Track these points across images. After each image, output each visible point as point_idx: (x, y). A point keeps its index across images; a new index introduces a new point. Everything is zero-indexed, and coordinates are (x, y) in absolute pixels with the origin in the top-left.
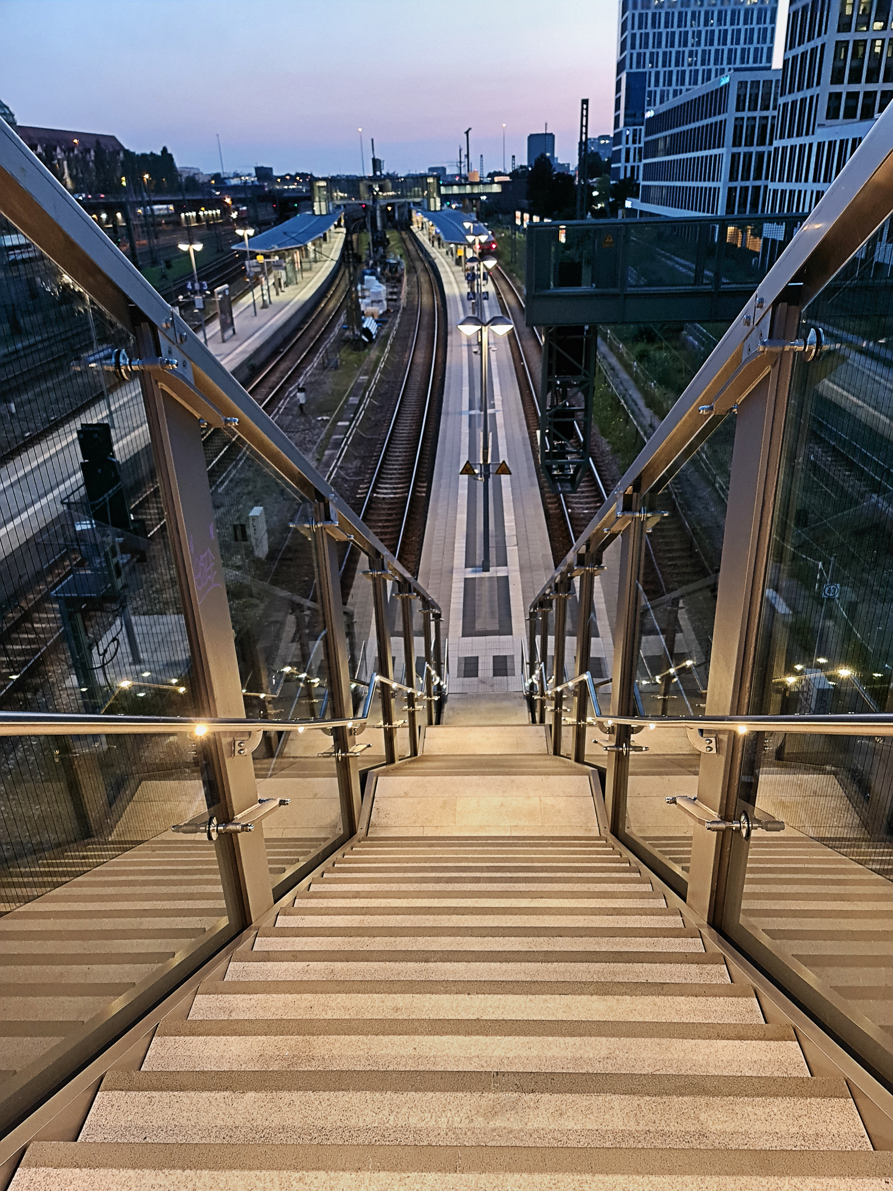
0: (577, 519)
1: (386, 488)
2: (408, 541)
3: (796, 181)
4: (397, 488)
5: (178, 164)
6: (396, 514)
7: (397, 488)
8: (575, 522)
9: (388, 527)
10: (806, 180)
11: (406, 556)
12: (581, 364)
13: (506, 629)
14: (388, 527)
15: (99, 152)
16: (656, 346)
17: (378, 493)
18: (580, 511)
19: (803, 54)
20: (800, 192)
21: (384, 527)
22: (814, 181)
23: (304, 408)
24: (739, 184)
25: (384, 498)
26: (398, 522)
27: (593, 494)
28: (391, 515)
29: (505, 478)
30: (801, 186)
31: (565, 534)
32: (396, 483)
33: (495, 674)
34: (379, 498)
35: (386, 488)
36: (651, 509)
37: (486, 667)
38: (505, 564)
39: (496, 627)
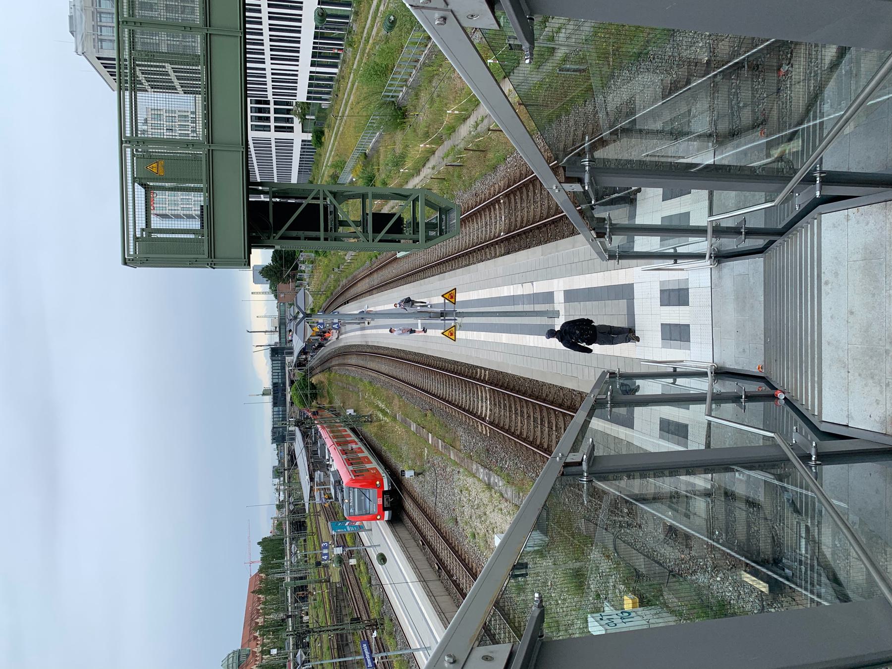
0: (510, 225)
1: (482, 407)
2: (529, 392)
3: (265, 77)
4: (482, 397)
5: (268, 534)
6: (504, 400)
7: (482, 397)
8: (513, 228)
9: (516, 410)
10: (264, 69)
11: (544, 395)
12: (301, 204)
13: (625, 292)
14: (516, 410)
15: (260, 591)
16: (377, 174)
17: (486, 416)
18: (503, 223)
19: (178, 79)
20: (273, 74)
21: (516, 414)
22: (264, 63)
23: (418, 471)
24: (272, 124)
25: (491, 410)
26: (512, 398)
27: (488, 213)
28: (505, 405)
29: (459, 297)
30: (268, 73)
31: (524, 236)
32: (478, 398)
33: (686, 303)
34: (490, 415)
35: (482, 407)
36: (643, 602)
37: (675, 315)
38: (551, 294)
39: (623, 303)
